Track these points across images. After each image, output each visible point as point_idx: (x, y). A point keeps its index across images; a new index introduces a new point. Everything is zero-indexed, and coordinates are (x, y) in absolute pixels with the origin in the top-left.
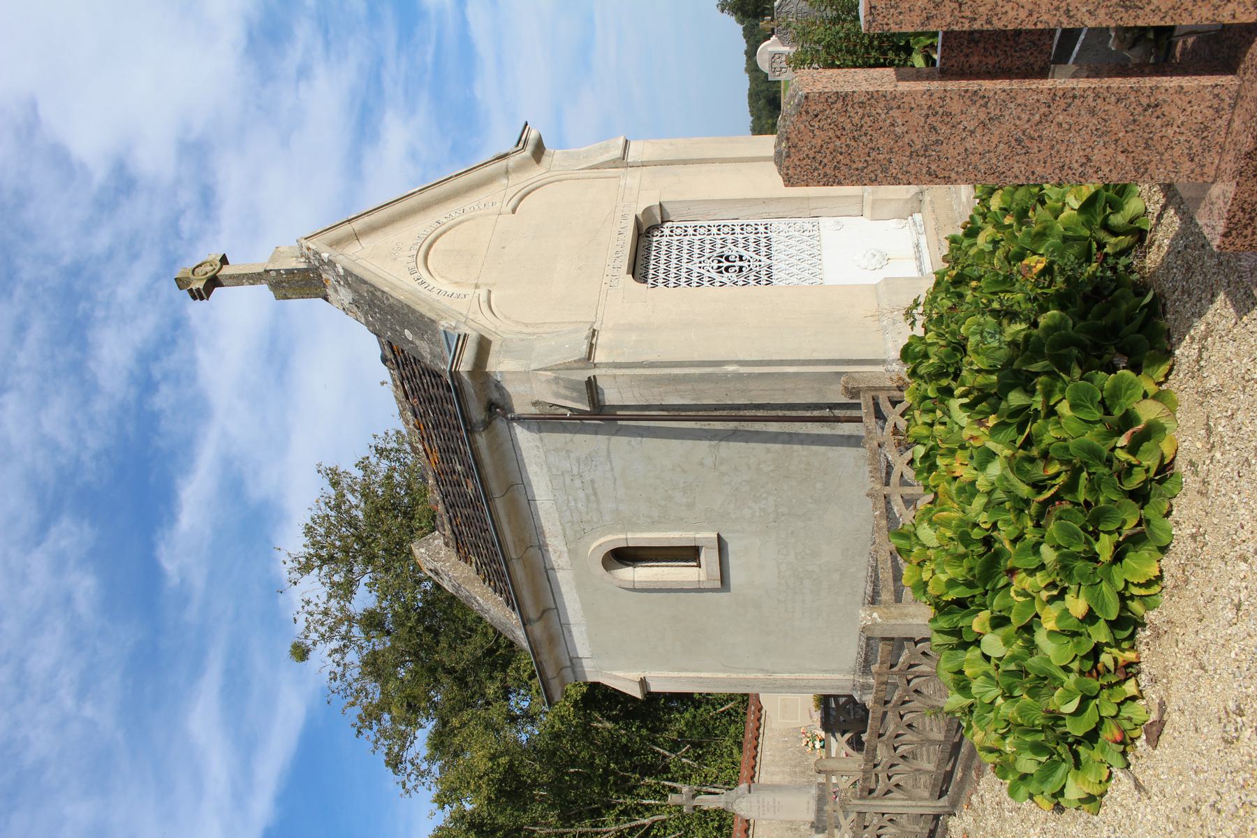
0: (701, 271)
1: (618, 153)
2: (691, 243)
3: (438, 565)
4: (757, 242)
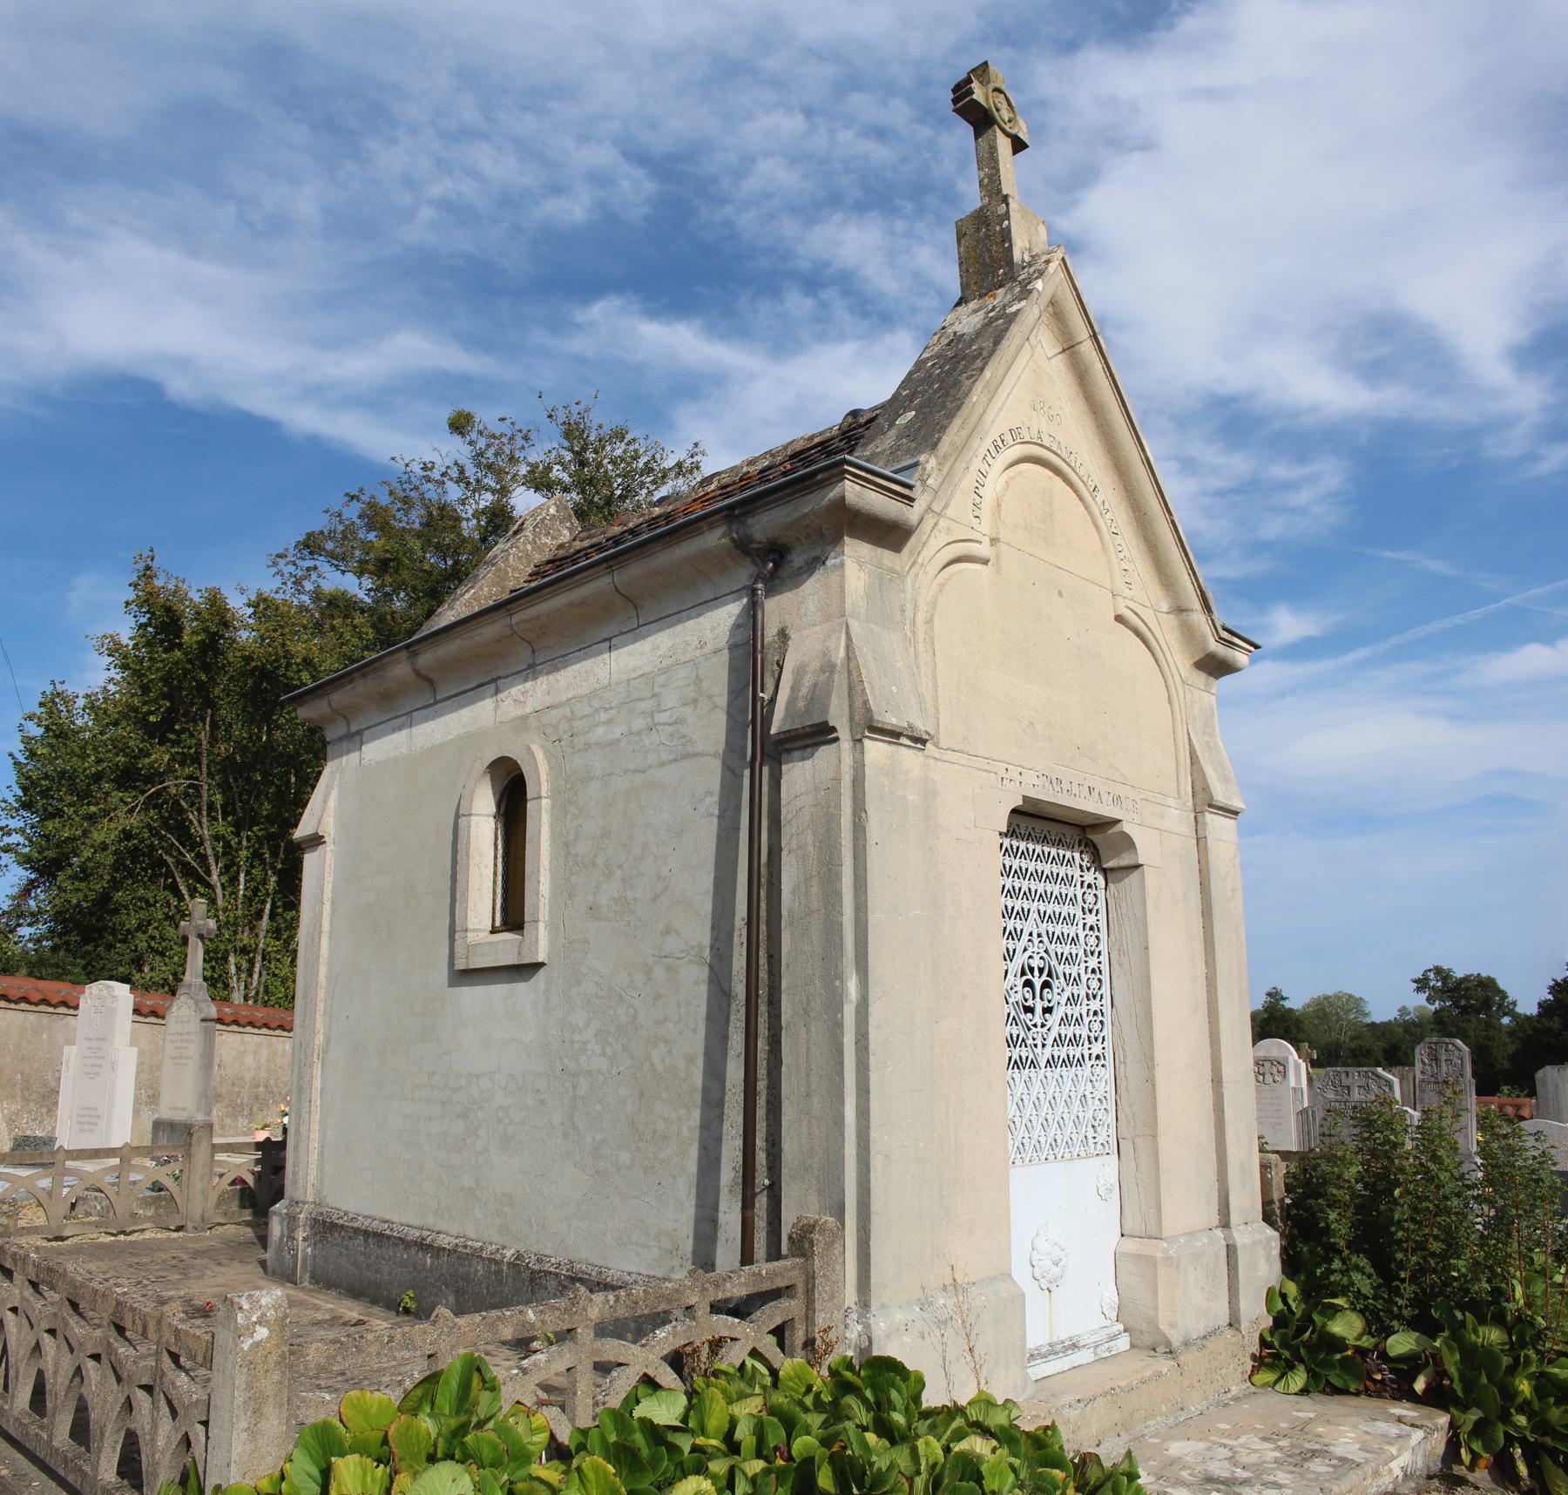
0: (1025, 937)
1: (1220, 797)
2: (1070, 920)
3: (528, 533)
4: (1075, 1041)
